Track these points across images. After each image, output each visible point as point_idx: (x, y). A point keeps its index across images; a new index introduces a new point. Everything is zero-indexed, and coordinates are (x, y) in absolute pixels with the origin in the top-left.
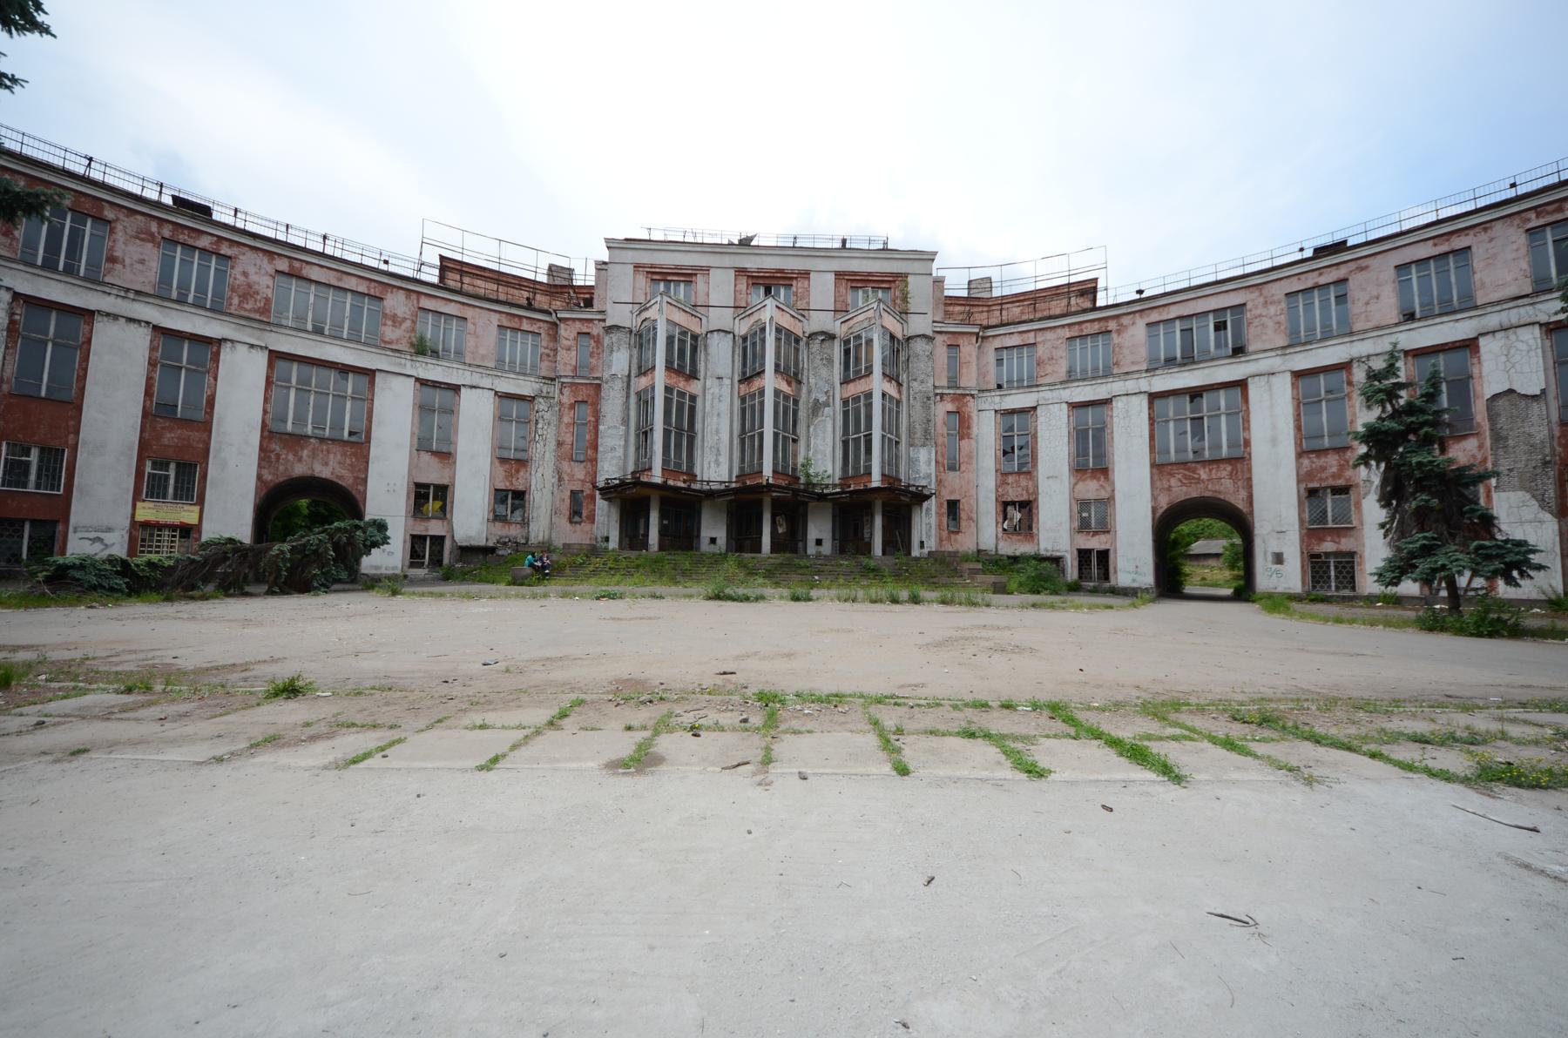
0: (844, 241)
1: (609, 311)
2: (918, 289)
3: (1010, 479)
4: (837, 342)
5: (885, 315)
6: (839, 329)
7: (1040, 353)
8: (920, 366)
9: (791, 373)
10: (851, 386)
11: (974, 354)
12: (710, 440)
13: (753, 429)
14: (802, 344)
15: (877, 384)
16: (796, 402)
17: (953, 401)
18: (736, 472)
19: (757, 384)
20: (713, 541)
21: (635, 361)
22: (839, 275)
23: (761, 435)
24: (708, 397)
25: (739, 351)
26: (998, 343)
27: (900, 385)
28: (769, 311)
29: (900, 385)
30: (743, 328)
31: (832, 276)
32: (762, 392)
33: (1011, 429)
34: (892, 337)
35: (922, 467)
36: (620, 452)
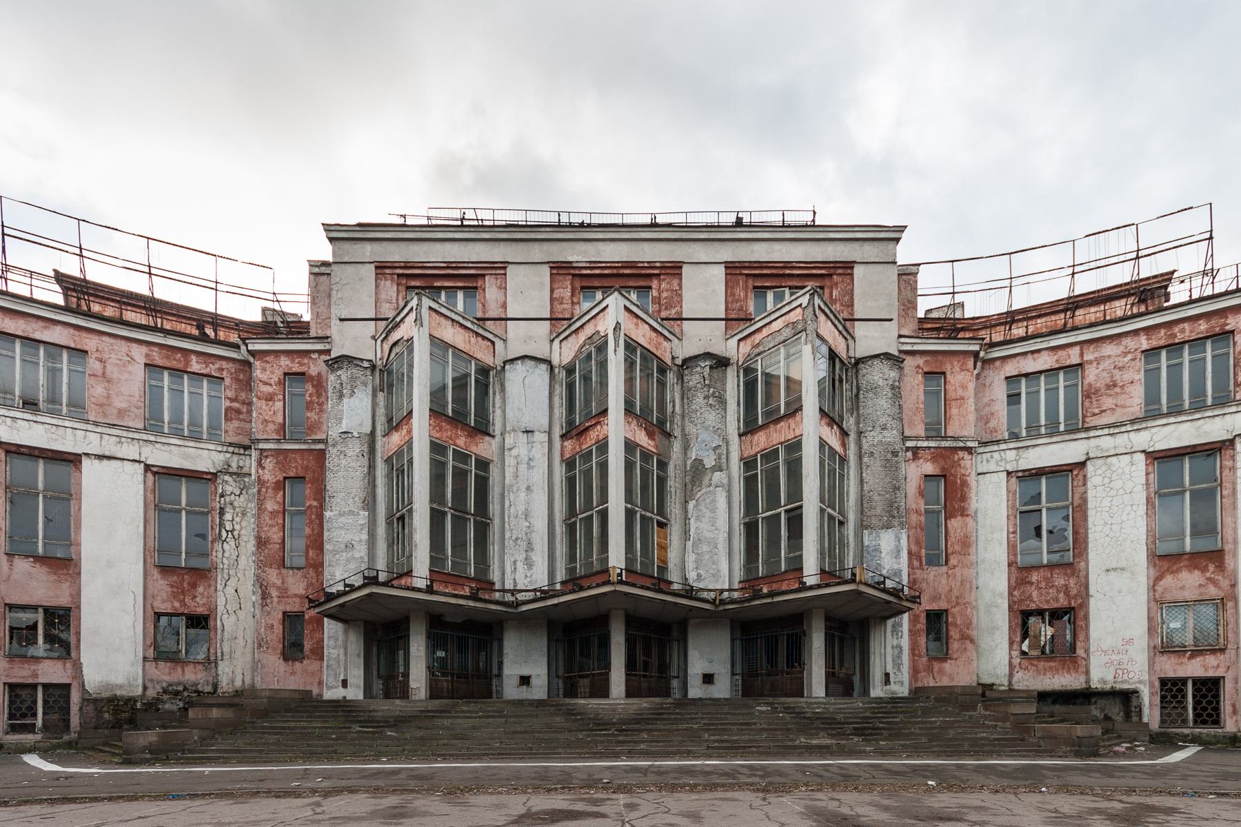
3: (1035, 577)
4: (731, 373)
5: (822, 317)
8: (878, 406)
9: (651, 417)
12: (515, 528)
13: (588, 505)
14: (671, 377)
16: (662, 465)
17: (934, 459)
20: (525, 680)
23: (604, 515)
27: (844, 434)
30: (565, 353)
31: (720, 271)
32: (603, 446)
33: (1037, 498)
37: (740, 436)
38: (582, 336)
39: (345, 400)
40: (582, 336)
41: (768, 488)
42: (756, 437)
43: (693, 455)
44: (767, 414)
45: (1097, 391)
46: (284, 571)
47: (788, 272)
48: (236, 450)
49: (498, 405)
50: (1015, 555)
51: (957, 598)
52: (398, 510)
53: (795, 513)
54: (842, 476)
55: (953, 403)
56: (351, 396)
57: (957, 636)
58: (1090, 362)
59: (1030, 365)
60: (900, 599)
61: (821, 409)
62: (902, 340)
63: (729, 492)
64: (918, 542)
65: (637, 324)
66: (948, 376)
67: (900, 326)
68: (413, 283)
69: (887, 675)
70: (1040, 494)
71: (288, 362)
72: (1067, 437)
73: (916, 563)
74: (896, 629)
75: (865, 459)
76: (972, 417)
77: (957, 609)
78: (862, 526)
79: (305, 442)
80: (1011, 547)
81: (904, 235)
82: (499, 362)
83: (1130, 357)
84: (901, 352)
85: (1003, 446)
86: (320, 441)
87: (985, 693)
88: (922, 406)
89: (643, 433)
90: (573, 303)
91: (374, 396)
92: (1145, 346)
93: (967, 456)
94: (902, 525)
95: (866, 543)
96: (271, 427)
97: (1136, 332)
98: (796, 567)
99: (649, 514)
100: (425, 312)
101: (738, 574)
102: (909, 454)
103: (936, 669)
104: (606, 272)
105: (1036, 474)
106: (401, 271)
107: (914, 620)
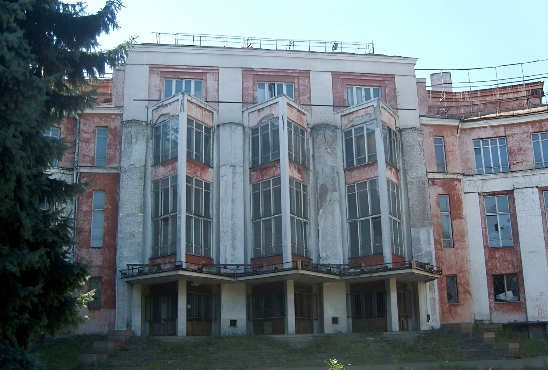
0: (336, 46)
1: (126, 105)
2: (407, 95)
3: (497, 255)
4: (339, 132)
5: (383, 111)
6: (334, 118)
7: (510, 145)
9: (300, 163)
10: (356, 173)
11: (457, 144)
14: (307, 135)
15: (383, 173)
16: (305, 187)
17: (442, 186)
18: (250, 255)
19: (269, 176)
20: (233, 323)
21: (151, 151)
22: (334, 74)
23: (279, 221)
24: (222, 183)
25: (249, 141)
26: (475, 135)
27: (397, 171)
28: (282, 109)
29: (397, 171)
30: (252, 120)
31: (329, 76)
32: (278, 181)
33: (493, 209)
34: (390, 130)
35: (425, 244)
36: (139, 239)
37: (345, 170)
38: (263, 114)
39: (134, 146)
40: (263, 114)
41: (362, 206)
42: (354, 173)
43: (320, 182)
44: (359, 161)
45: (514, 152)
46: (90, 250)
47: (363, 78)
48: (65, 172)
49: (215, 149)
50: (487, 241)
51: (461, 268)
52: (161, 215)
53: (376, 220)
54: (398, 195)
55: (449, 154)
56: (136, 143)
57: (463, 291)
58: (509, 136)
59: (484, 134)
60: (432, 273)
61: (386, 162)
62: (422, 118)
63: (341, 204)
64: (438, 235)
65: (292, 111)
66: (445, 137)
67: (420, 110)
68: (168, 76)
69: (428, 316)
70: (495, 206)
71: (98, 120)
72: (504, 175)
73: (439, 247)
74: (431, 288)
75: (409, 186)
76: (459, 161)
77: (461, 274)
78: (409, 226)
79: (106, 168)
80: (485, 236)
81: (417, 62)
82: (215, 124)
83: (526, 135)
84: (422, 124)
85: (475, 178)
86: (115, 168)
87: (478, 325)
88: (434, 155)
89: (296, 171)
90: (253, 90)
91: (147, 142)
92: (531, 131)
93: (459, 184)
94: (430, 224)
95: (413, 235)
96: (87, 159)
97: (526, 123)
98: (380, 254)
99: (300, 219)
100: (186, 102)
101: (348, 254)
102: (430, 182)
103: (453, 311)
104: (271, 74)
105: (492, 195)
106: (163, 70)
107: (440, 283)
